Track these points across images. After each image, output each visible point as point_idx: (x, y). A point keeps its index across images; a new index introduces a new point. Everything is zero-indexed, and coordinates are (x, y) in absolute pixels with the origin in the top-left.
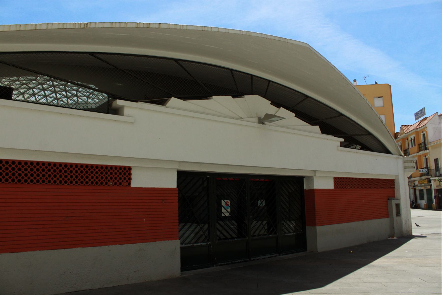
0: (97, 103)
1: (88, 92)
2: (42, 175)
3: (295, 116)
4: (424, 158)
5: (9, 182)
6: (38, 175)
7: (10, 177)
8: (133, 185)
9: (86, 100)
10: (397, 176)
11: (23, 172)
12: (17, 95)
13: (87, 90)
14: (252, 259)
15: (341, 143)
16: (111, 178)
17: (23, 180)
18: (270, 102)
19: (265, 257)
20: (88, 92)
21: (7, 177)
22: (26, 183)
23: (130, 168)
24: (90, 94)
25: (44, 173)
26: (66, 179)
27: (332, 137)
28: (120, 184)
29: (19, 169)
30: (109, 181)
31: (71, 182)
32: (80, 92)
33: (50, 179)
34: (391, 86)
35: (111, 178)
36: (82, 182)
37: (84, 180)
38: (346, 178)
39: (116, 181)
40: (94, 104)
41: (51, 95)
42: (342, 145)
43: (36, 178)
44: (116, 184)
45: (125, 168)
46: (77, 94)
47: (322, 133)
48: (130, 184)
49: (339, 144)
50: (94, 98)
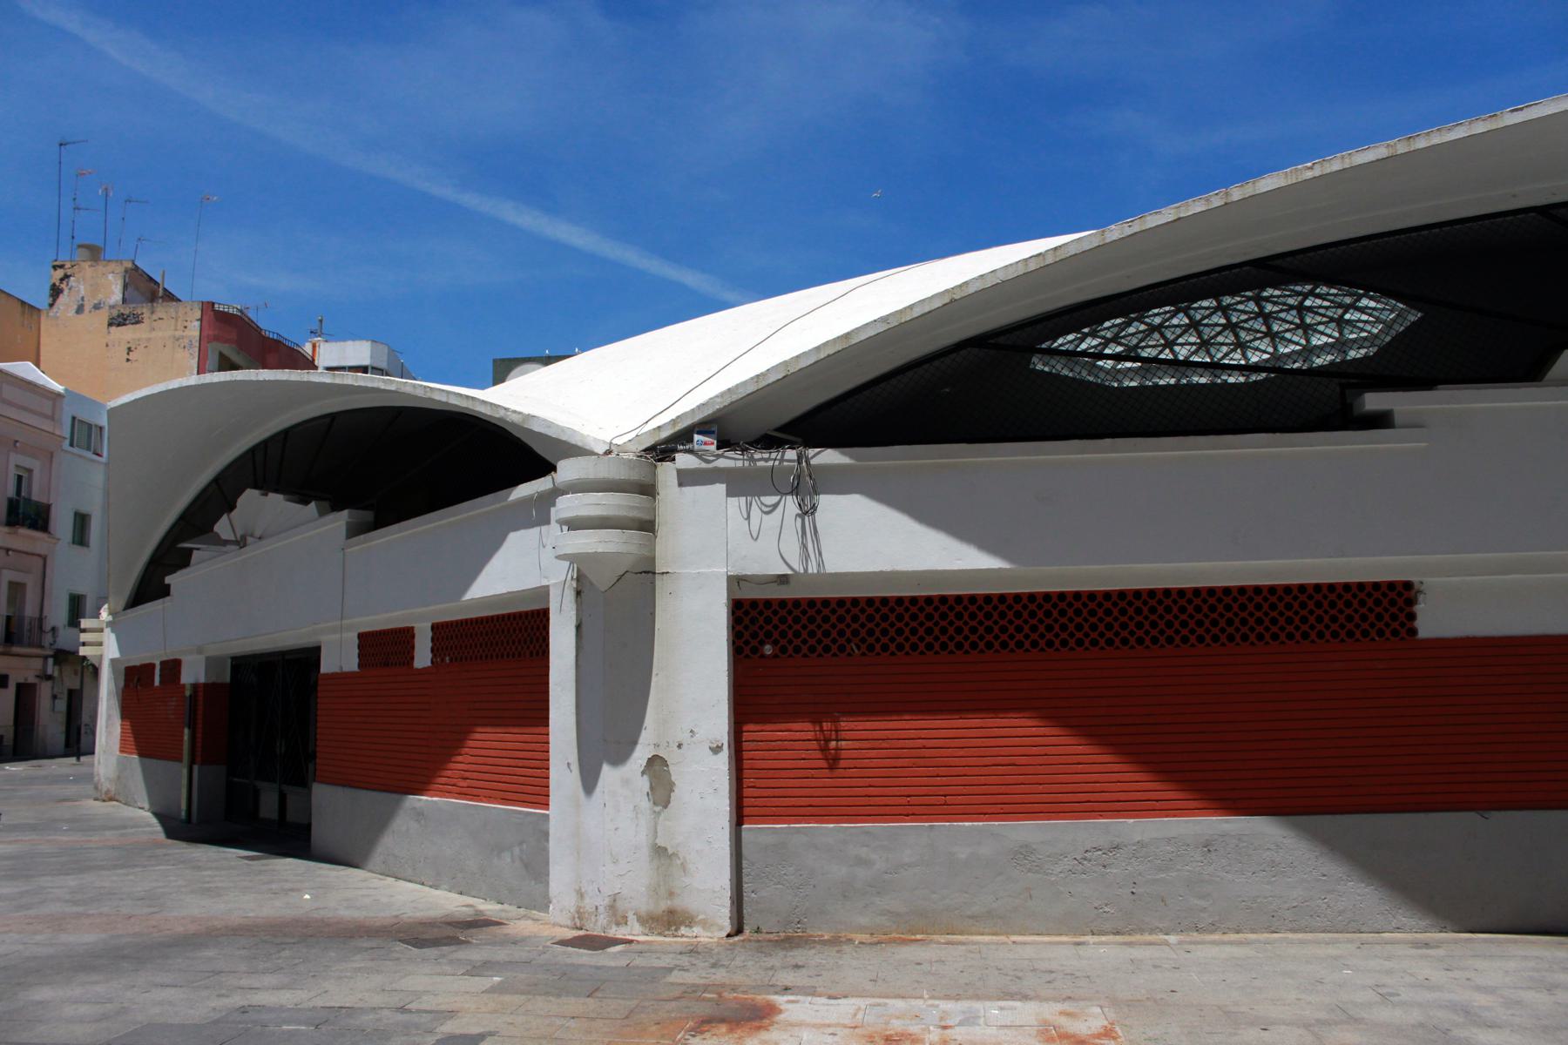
0: (1376, 336)
1: (1298, 294)
2: (815, 636)
5: (1130, 645)
6: (1230, 622)
7: (951, 638)
9: (1213, 351)
11: (1341, 611)
12: (1160, 349)
13: (1298, 288)
17: (1142, 635)
20: (1298, 294)
21: (944, 638)
22: (976, 652)
24: (1306, 296)
25: (1017, 622)
26: (914, 639)
28: (842, 649)
30: (849, 641)
31: (827, 649)
32: (1267, 299)
33: (1034, 636)
35: (855, 633)
37: (907, 639)
38: (469, 623)
40: (1144, 371)
41: (1180, 339)
43: (922, 642)
44: (783, 650)
46: (1261, 308)
48: (1413, 632)
50: (1375, 322)
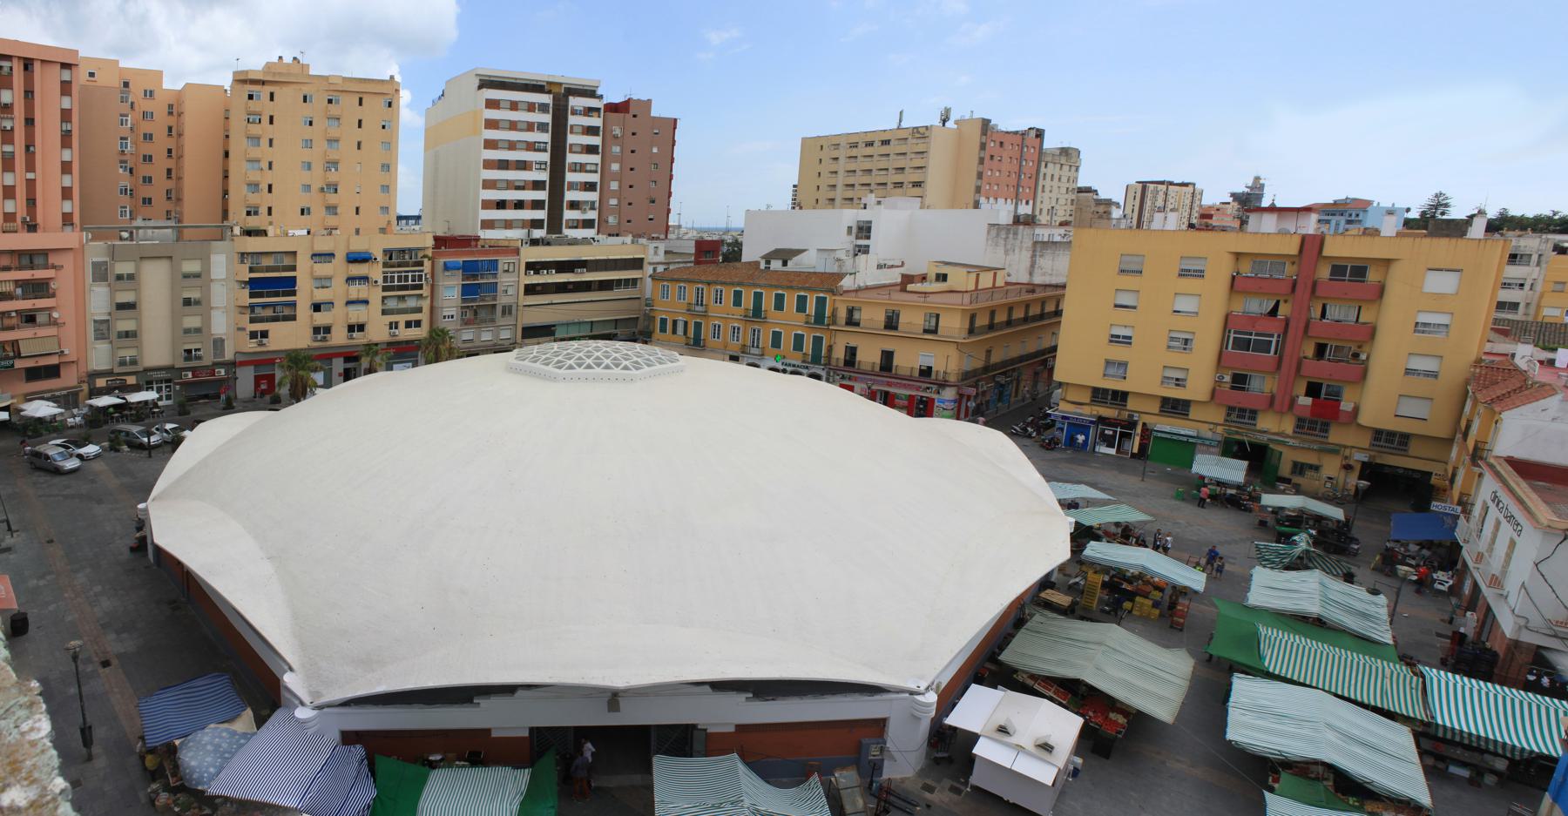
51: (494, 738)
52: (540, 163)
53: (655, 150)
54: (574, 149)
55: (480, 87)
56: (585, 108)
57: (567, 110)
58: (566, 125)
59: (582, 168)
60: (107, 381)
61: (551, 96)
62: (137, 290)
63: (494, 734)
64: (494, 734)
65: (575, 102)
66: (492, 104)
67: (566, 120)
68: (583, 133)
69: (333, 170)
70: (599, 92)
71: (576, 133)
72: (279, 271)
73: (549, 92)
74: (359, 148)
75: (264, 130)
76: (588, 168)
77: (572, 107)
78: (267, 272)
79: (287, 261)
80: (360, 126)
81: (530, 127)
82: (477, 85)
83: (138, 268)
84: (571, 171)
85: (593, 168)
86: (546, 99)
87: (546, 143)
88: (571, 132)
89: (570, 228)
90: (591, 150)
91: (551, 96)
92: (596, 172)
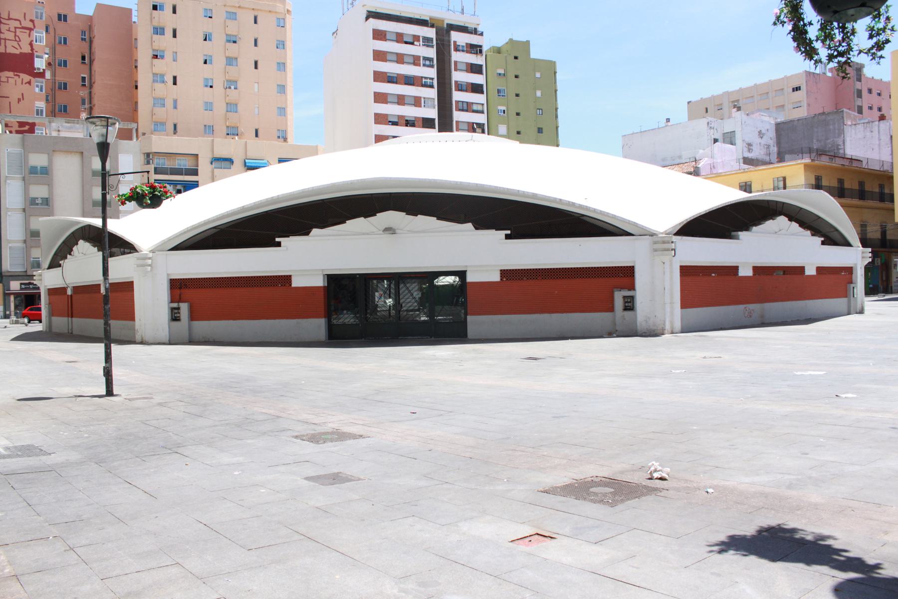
3: (813, 235)
4: (6, 151)
8: (293, 285)
10: (856, 265)
14: (400, 338)
15: (822, 241)
16: (540, 275)
18: (436, 218)
19: (415, 337)
23: (290, 276)
27: (492, 232)
29: (554, 272)
34: (172, 12)
36: (566, 278)
39: (507, 278)
42: (823, 243)
45: (287, 276)
47: (476, 228)
48: (291, 285)
49: (820, 243)
51: (298, 289)
52: (425, 59)
53: (539, 93)
54: (459, 66)
55: (367, 18)
56: (467, 44)
57: (449, 46)
58: (452, 121)
59: (467, 107)
60: (21, 284)
61: (434, 30)
62: (50, 185)
63: (296, 283)
64: (296, 283)
65: (455, 36)
66: (379, 35)
67: (450, 56)
68: (467, 71)
69: (233, 87)
70: (480, 29)
71: (463, 130)
72: (182, 174)
73: (432, 26)
74: (256, 67)
75: (165, 42)
76: (475, 107)
77: (456, 82)
78: (171, 174)
79: (186, 164)
80: (256, 45)
81: (416, 60)
82: (365, 16)
83: (50, 161)
84: (458, 110)
85: (479, 108)
86: (431, 33)
87: (432, 79)
88: (456, 70)
89: (460, 110)
90: (476, 89)
91: (434, 30)
92: (482, 112)
